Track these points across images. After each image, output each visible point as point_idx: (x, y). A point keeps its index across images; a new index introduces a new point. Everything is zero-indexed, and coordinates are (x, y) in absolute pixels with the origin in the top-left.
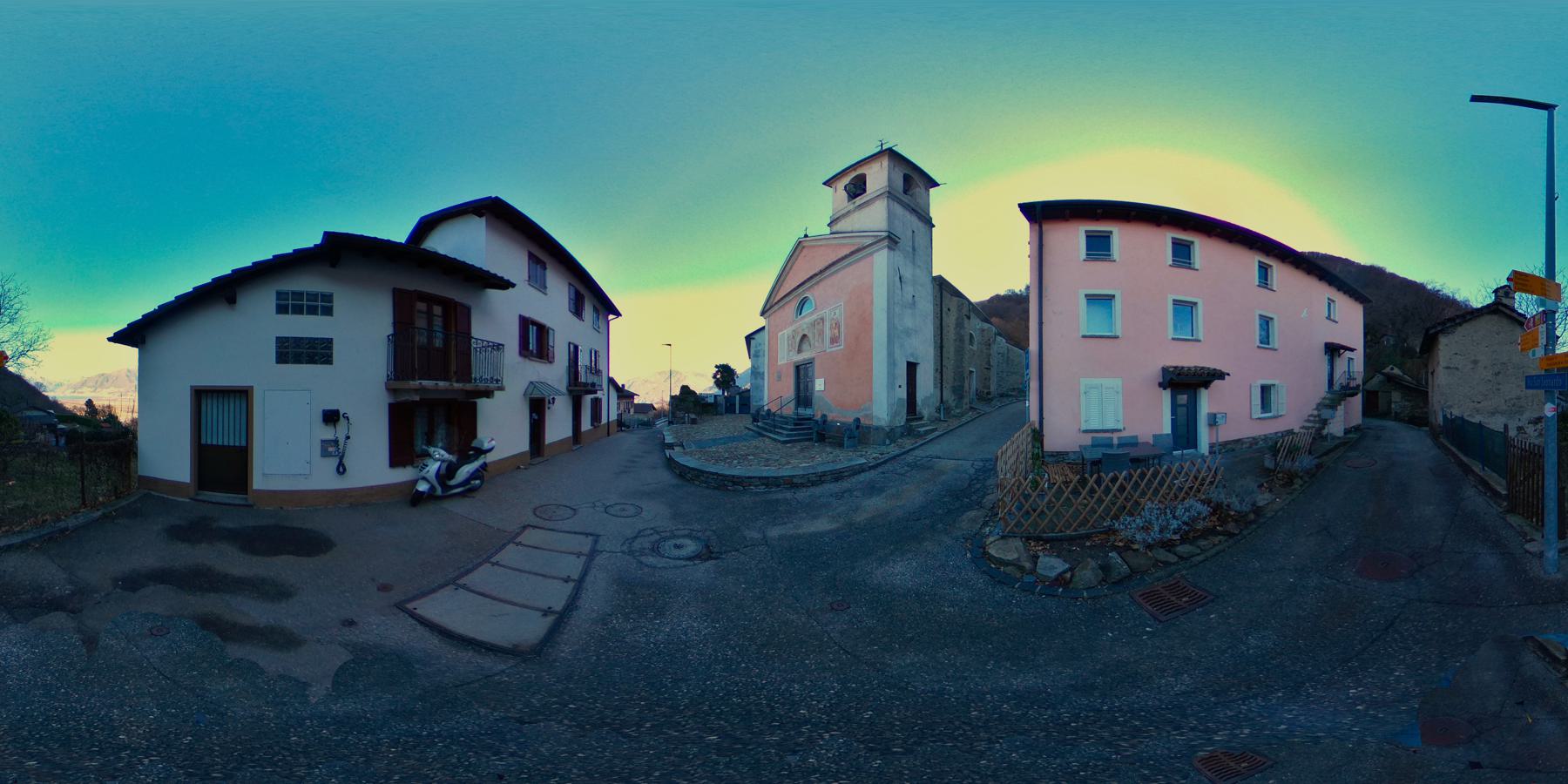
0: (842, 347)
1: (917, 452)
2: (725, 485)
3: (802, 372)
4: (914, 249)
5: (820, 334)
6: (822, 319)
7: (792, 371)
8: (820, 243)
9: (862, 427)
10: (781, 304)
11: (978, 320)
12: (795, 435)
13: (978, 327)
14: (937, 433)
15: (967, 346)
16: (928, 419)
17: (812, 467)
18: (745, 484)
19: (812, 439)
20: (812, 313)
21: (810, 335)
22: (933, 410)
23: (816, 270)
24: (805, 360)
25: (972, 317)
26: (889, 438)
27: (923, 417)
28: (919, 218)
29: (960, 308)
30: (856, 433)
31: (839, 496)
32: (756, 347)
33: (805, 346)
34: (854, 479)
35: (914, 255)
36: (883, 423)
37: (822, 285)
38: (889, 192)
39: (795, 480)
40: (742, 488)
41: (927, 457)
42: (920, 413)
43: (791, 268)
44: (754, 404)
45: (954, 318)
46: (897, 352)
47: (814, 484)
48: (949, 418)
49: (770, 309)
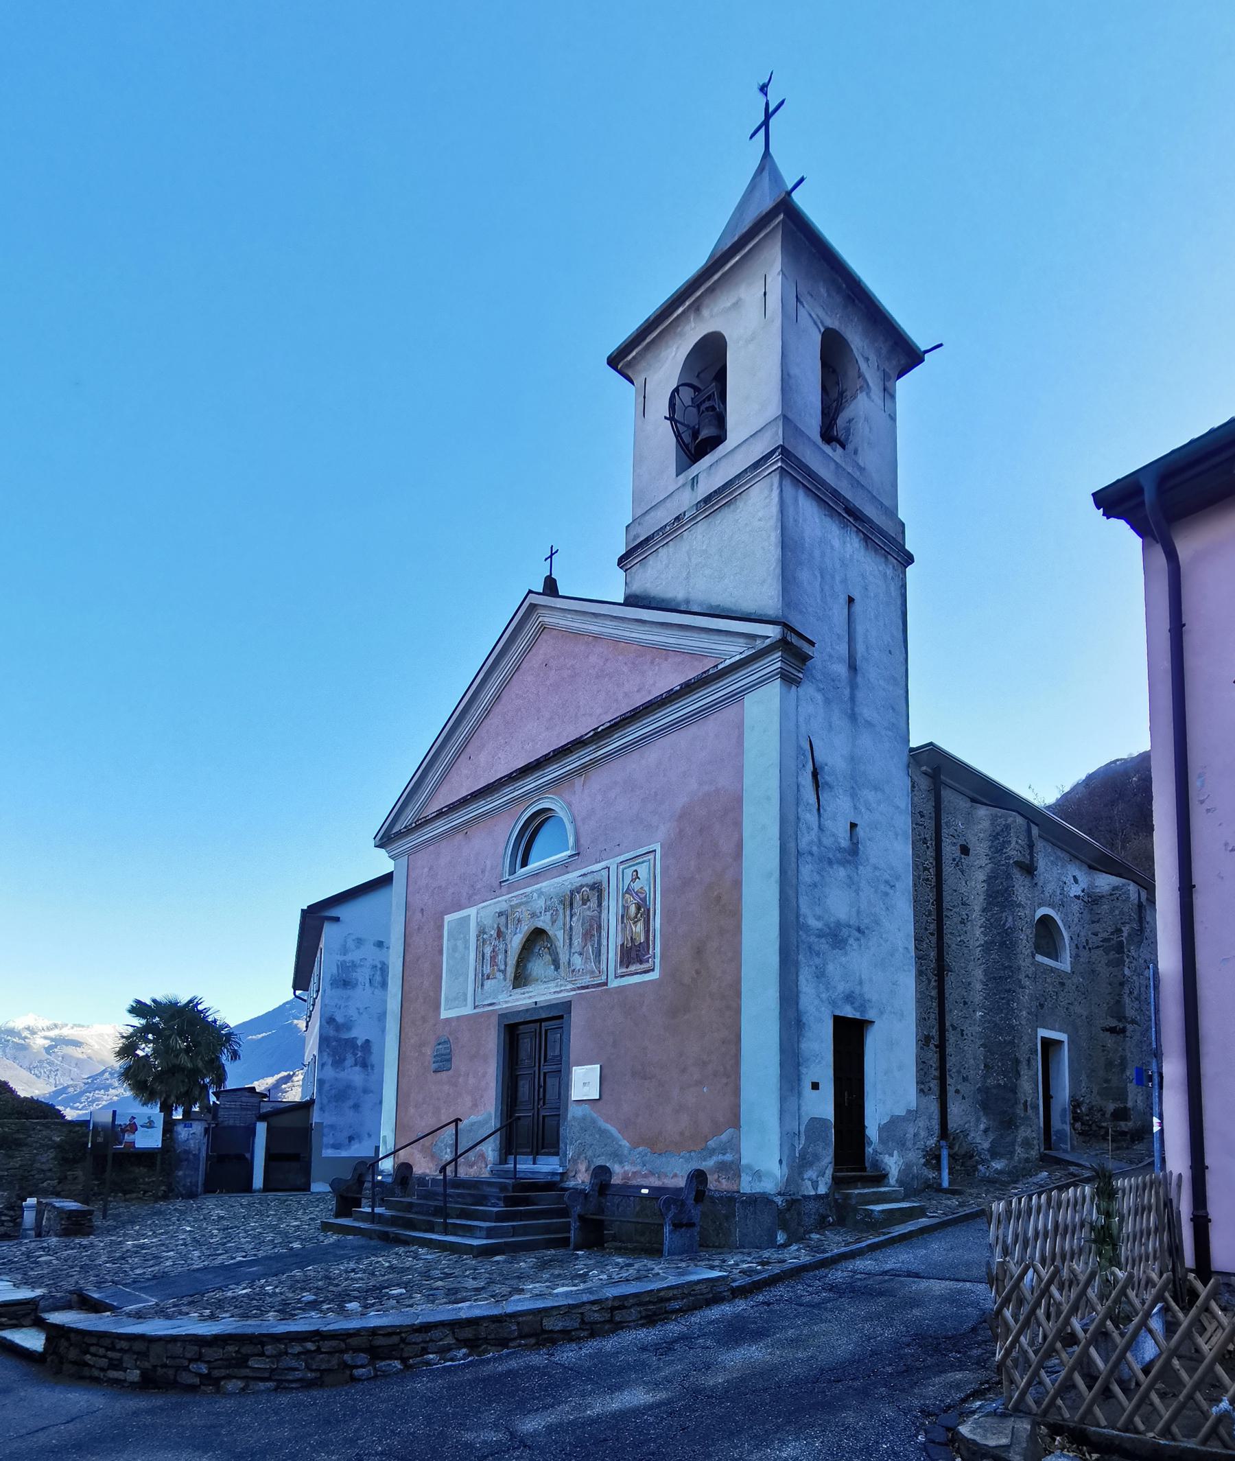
0: (654, 976)
1: (862, 1264)
2: (345, 1366)
3: (526, 1045)
4: (853, 667)
5: (587, 935)
6: (597, 888)
7: (491, 1042)
9: (712, 1197)
11: (1074, 870)
12: (515, 1231)
13: (1075, 890)
14: (924, 1222)
15: (1027, 958)
16: (900, 1182)
17: (589, 1291)
18: (408, 1351)
19: (564, 1243)
20: (564, 867)
21: (558, 935)
22: (915, 1156)
23: (584, 728)
24: (536, 1007)
25: (1042, 863)
26: (785, 1228)
28: (866, 539)
30: (696, 1213)
31: (666, 1348)
32: (345, 951)
33: (539, 966)
34: (696, 1318)
35: (853, 686)
36: (768, 1186)
37: (600, 778)
39: (549, 1324)
40: (398, 1364)
41: (885, 1273)
42: (876, 1164)
44: (328, 1153)
45: (981, 876)
47: (595, 1333)
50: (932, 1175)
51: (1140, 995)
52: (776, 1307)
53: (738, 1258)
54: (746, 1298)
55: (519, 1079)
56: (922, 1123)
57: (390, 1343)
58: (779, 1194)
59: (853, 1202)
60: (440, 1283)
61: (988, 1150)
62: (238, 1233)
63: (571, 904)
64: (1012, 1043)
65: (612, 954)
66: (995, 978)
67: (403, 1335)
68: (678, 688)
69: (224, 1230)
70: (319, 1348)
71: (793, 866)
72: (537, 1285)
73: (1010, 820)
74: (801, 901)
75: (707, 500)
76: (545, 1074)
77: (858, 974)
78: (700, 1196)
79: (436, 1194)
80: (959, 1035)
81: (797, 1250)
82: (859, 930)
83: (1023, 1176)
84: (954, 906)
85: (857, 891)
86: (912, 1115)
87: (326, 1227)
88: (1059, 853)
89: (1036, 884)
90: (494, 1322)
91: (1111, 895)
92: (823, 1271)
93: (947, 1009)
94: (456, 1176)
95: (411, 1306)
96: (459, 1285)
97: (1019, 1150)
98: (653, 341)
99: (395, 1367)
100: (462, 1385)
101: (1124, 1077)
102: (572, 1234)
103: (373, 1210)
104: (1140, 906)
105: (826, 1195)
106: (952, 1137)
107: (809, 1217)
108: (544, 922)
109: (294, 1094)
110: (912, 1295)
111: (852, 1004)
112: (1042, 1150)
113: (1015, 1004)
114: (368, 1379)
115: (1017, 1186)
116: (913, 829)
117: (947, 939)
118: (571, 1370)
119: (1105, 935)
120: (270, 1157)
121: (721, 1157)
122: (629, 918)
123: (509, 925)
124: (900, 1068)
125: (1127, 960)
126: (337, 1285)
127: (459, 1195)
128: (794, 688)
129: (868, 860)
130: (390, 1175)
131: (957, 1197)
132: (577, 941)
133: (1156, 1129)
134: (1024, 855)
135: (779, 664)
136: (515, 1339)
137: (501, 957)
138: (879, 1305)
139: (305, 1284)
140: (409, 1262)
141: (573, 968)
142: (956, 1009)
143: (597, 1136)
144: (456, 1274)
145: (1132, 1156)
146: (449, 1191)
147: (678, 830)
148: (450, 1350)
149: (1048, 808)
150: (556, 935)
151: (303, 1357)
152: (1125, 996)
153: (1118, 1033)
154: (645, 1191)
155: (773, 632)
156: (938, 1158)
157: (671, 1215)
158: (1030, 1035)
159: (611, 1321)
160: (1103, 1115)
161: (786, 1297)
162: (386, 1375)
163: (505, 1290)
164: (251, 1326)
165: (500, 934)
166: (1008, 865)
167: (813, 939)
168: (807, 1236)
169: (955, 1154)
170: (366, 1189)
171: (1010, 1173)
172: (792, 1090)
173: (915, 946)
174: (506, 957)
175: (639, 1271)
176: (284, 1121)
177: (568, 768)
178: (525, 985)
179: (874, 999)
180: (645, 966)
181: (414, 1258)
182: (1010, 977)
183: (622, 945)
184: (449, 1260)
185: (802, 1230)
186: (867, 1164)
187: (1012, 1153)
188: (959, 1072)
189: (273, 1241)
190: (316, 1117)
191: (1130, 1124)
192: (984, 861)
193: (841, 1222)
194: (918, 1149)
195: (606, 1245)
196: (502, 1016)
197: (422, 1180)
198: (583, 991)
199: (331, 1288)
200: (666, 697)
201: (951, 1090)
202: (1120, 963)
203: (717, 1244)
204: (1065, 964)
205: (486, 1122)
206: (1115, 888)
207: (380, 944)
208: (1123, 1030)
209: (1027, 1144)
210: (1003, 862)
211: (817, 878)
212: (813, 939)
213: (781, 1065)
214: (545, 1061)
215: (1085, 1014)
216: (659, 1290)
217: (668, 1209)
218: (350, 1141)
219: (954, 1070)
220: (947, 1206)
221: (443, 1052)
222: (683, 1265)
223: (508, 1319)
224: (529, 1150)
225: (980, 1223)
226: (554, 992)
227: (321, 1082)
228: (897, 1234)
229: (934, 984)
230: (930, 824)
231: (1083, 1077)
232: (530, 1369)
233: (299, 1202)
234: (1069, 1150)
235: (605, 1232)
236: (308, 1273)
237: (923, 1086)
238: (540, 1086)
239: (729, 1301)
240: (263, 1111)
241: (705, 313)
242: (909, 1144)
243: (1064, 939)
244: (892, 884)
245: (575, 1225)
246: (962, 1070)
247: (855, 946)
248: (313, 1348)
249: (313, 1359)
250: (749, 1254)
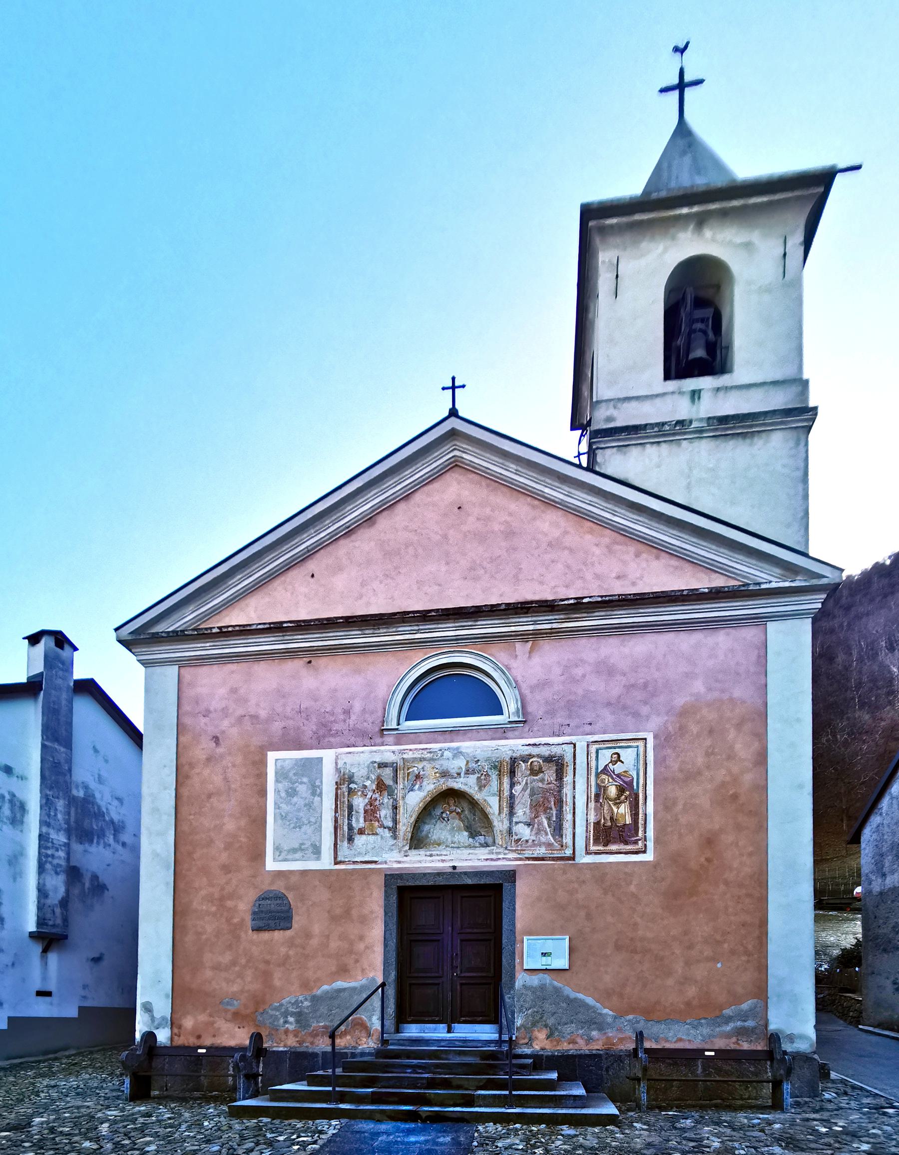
5: (538, 806)
68: (706, 590)
75: (724, 420)
98: (640, 223)
132: (522, 812)
147: (678, 725)
165: (381, 786)
177: (513, 629)
183: (597, 824)
226: (487, 860)
241: (708, 233)
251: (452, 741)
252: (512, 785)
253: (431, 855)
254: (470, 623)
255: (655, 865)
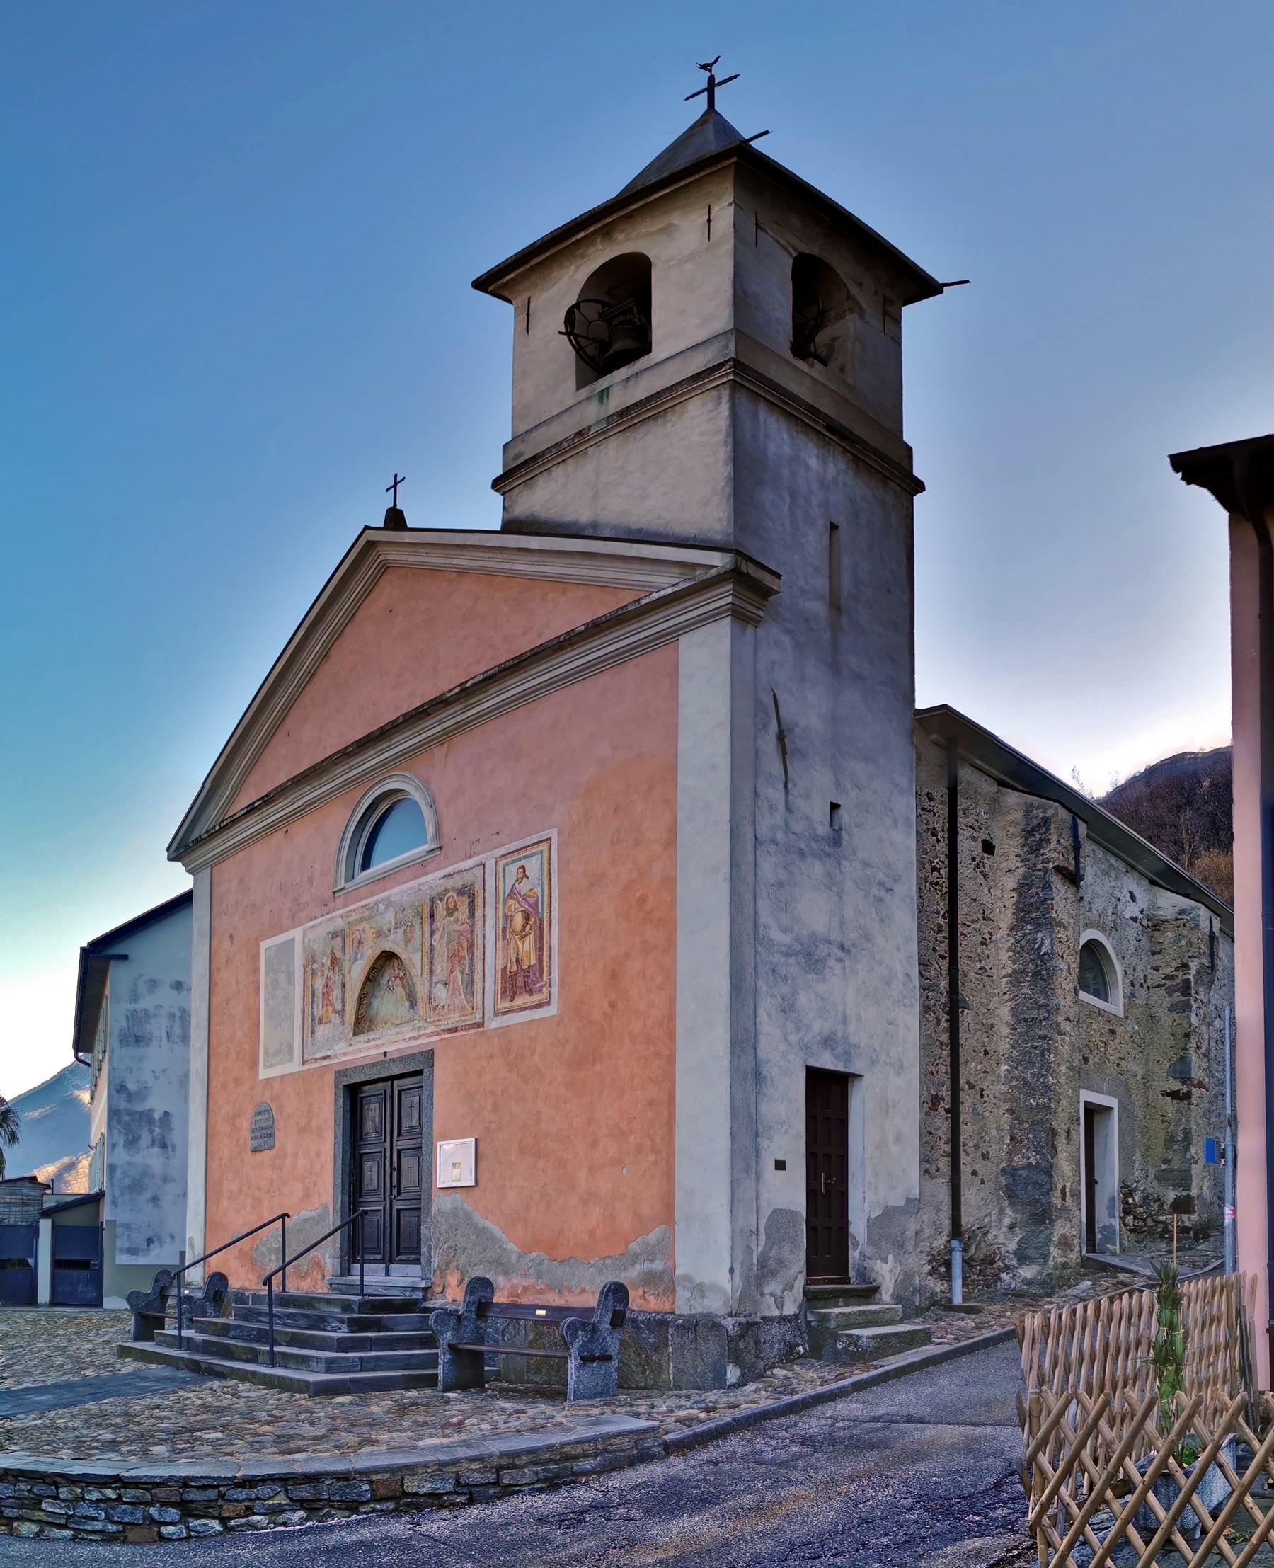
0: (551, 1011)
1: (841, 1408)
3: (373, 1113)
5: (454, 957)
6: (467, 892)
8: (459, 562)
9: (635, 1321)
10: (274, 813)
11: (1131, 883)
12: (364, 1365)
13: (1131, 910)
16: (898, 1298)
19: (431, 1382)
20: (421, 865)
21: (413, 959)
23: (446, 683)
25: (1089, 872)
26: (738, 1361)
27: (876, 1289)
28: (857, 461)
29: (1034, 835)
30: (612, 1342)
33: (388, 1003)
34: (615, 1481)
36: (715, 1305)
37: (466, 746)
38: (738, 365)
39: (411, 1485)
40: (216, 1525)
41: (877, 1419)
42: (863, 1274)
43: (325, 656)
44: (123, 1259)
45: (1010, 882)
46: (769, 1027)
48: (992, 1301)
49: (212, 835)
50: (939, 1287)
51: (1208, 1050)
52: (727, 1467)
53: (672, 1402)
54: (684, 1455)
55: (364, 1159)
56: (927, 1216)
57: (205, 1498)
58: (730, 1315)
59: (833, 1324)
60: (267, 1428)
61: (1015, 1254)
62: (25, 1355)
63: (432, 916)
64: (1046, 1107)
65: (490, 983)
66: (1026, 1020)
67: (221, 1489)
68: (583, 628)
69: (9, 1350)
70: (120, 1497)
71: (750, 858)
72: (395, 1435)
73: (1050, 813)
74: (760, 903)
76: (399, 1152)
77: (840, 1009)
78: (618, 1320)
79: (260, 1314)
80: (978, 1096)
81: (756, 1391)
82: (842, 948)
83: (1061, 1287)
84: (973, 921)
85: (840, 896)
86: (913, 1205)
87: (124, 1352)
88: (1113, 860)
89: (1082, 898)
90: (339, 1479)
91: (1177, 919)
92: (791, 1419)
93: (962, 1060)
94: (284, 1290)
95: (231, 1454)
96: (292, 1432)
97: (1054, 1251)
99: (213, 1528)
100: (298, 1555)
101: (1188, 1156)
102: (440, 1370)
103: (180, 1333)
104: (1212, 936)
105: (796, 1317)
106: (966, 1236)
107: (772, 1347)
108: (395, 942)
109: (80, 1185)
110: (915, 1447)
111: (833, 1049)
112: (1084, 1252)
113: (1052, 1056)
114: (181, 1539)
115: (1053, 1300)
116: (918, 816)
117: (963, 963)
118: (444, 1543)
119: (1168, 971)
120: (57, 1264)
121: (647, 1266)
122: (513, 932)
123: (347, 949)
124: (898, 1140)
125: (1195, 1006)
126: (139, 1424)
127: (289, 1316)
128: (750, 629)
129: (854, 853)
130: (200, 1288)
131: (973, 1316)
132: (441, 966)
133: (1227, 1221)
134: (1068, 859)
135: (729, 599)
136: (367, 1502)
137: (336, 993)
138: (868, 1461)
139: (101, 1421)
140: (227, 1400)
141: (434, 1004)
142: (973, 1059)
143: (473, 1237)
144: (288, 1417)
145: (1196, 1259)
146: (276, 1310)
148: (283, 1511)
149: (1099, 802)
150: (410, 960)
151: (102, 1505)
152: (1192, 1052)
153: (1182, 1099)
154: (541, 1312)
155: (719, 561)
156: (948, 1264)
157: (577, 1344)
158: (1070, 1098)
159: (496, 1484)
160: (1161, 1206)
161: (741, 1453)
162: (202, 1537)
163: (353, 1440)
164: (44, 1464)
165: (334, 961)
166: (1046, 870)
167: (777, 958)
168: (769, 1373)
169: (971, 1259)
170: (170, 1307)
171: (1042, 1284)
172: (747, 1171)
173: (920, 972)
174: (343, 993)
175: (533, 1419)
176: (74, 1219)
177: (424, 736)
178: (370, 1030)
179: (862, 1045)
180: (536, 998)
181: (233, 1395)
182: (1045, 1018)
183: (504, 970)
184: (278, 1400)
185: (761, 1364)
186: (852, 1274)
187: (1045, 1256)
188: (977, 1146)
189: (62, 1366)
190: (107, 1213)
191: (1195, 1217)
192: (1014, 863)
193: (816, 1352)
194: (922, 1252)
195: (486, 1386)
196: (340, 1074)
197: (240, 1297)
198: (449, 1036)
199: (131, 1427)
200: (565, 640)
201: (965, 1171)
202: (1186, 1007)
203: (643, 1384)
204: (1116, 1005)
205: (321, 1218)
206: (1182, 912)
207: (178, 986)
208: (1188, 1096)
209: (1065, 1243)
210: (1039, 867)
211: (782, 875)
212: (777, 958)
213: (733, 1136)
214: (399, 1134)
215: (1140, 1073)
216: (563, 1445)
217: (575, 1336)
218: (148, 1245)
219: (971, 1144)
220: (959, 1328)
221: (264, 1124)
222: (596, 1411)
223: (357, 1476)
224: (379, 1257)
225: (1004, 1350)
226: (410, 1039)
227: (112, 1169)
228: (891, 1367)
229: (945, 1025)
230: (942, 810)
231: (1137, 1156)
232: (389, 1540)
233: (90, 1320)
234: (1118, 1252)
235: (486, 1368)
236: (104, 1407)
237: (928, 1166)
238: (392, 1169)
239: (660, 1459)
240: (46, 1205)
242: (909, 1246)
243: (1115, 972)
244: (888, 887)
245: (444, 1357)
246: (981, 1144)
247: (838, 968)
248: (114, 1497)
249: (113, 1508)
250: (688, 1397)
251: (385, 890)
252: (432, 933)
253: (368, 1041)
254: (385, 746)
255: (559, 1020)
